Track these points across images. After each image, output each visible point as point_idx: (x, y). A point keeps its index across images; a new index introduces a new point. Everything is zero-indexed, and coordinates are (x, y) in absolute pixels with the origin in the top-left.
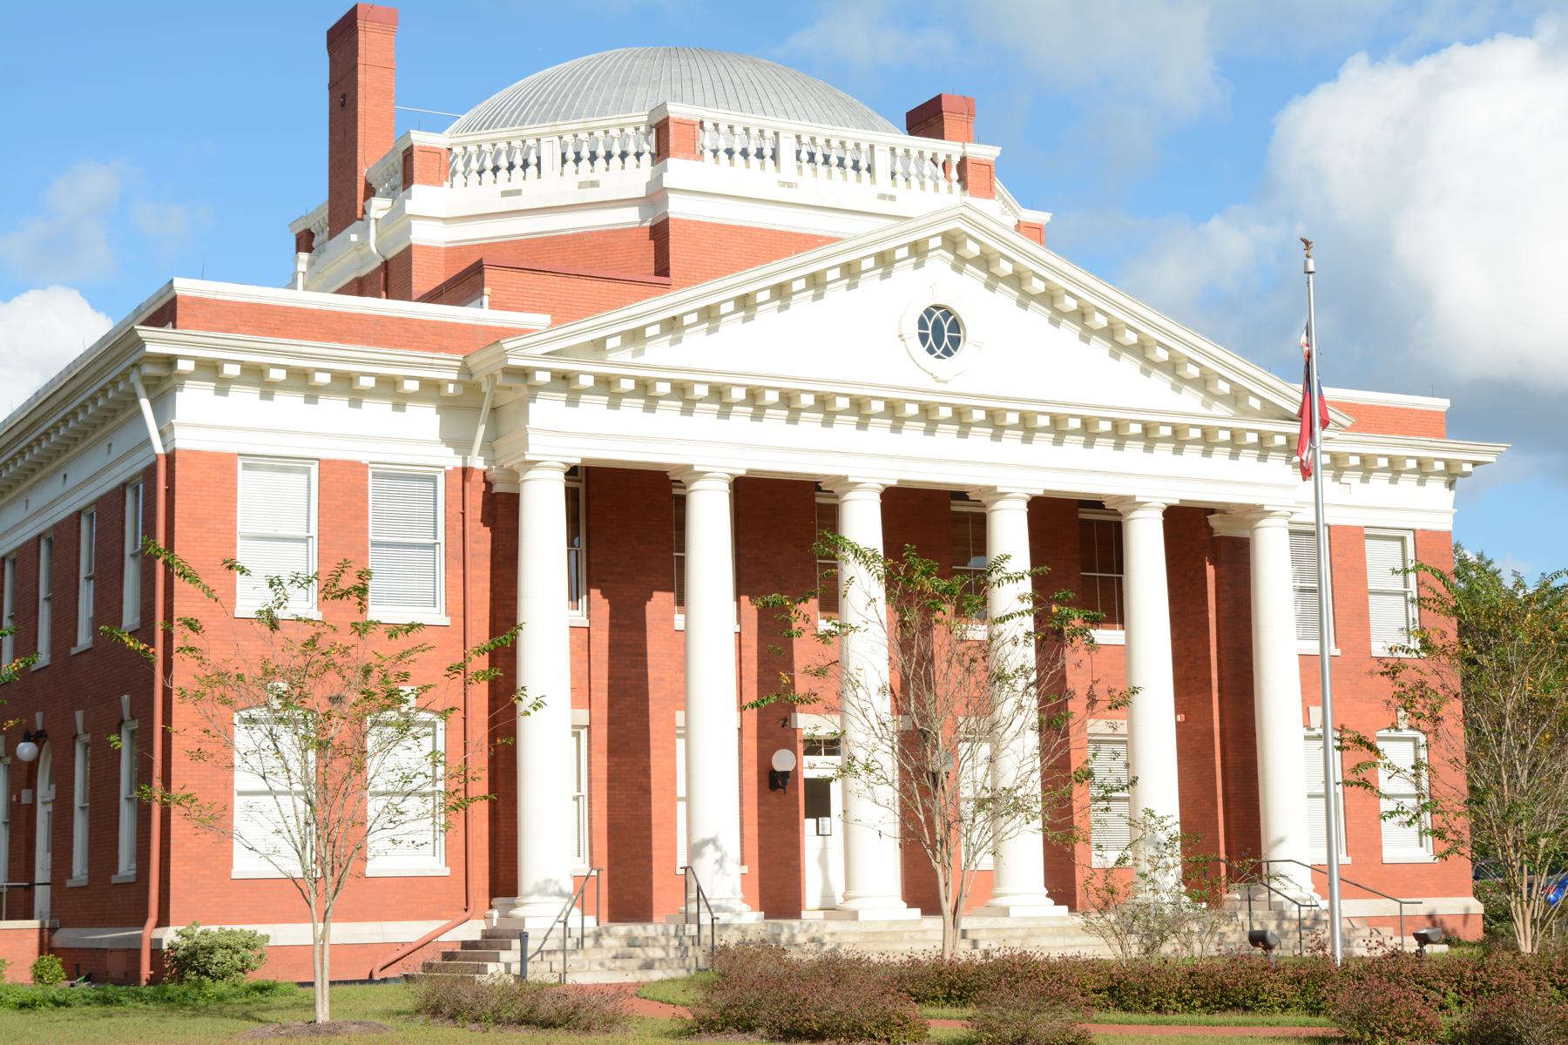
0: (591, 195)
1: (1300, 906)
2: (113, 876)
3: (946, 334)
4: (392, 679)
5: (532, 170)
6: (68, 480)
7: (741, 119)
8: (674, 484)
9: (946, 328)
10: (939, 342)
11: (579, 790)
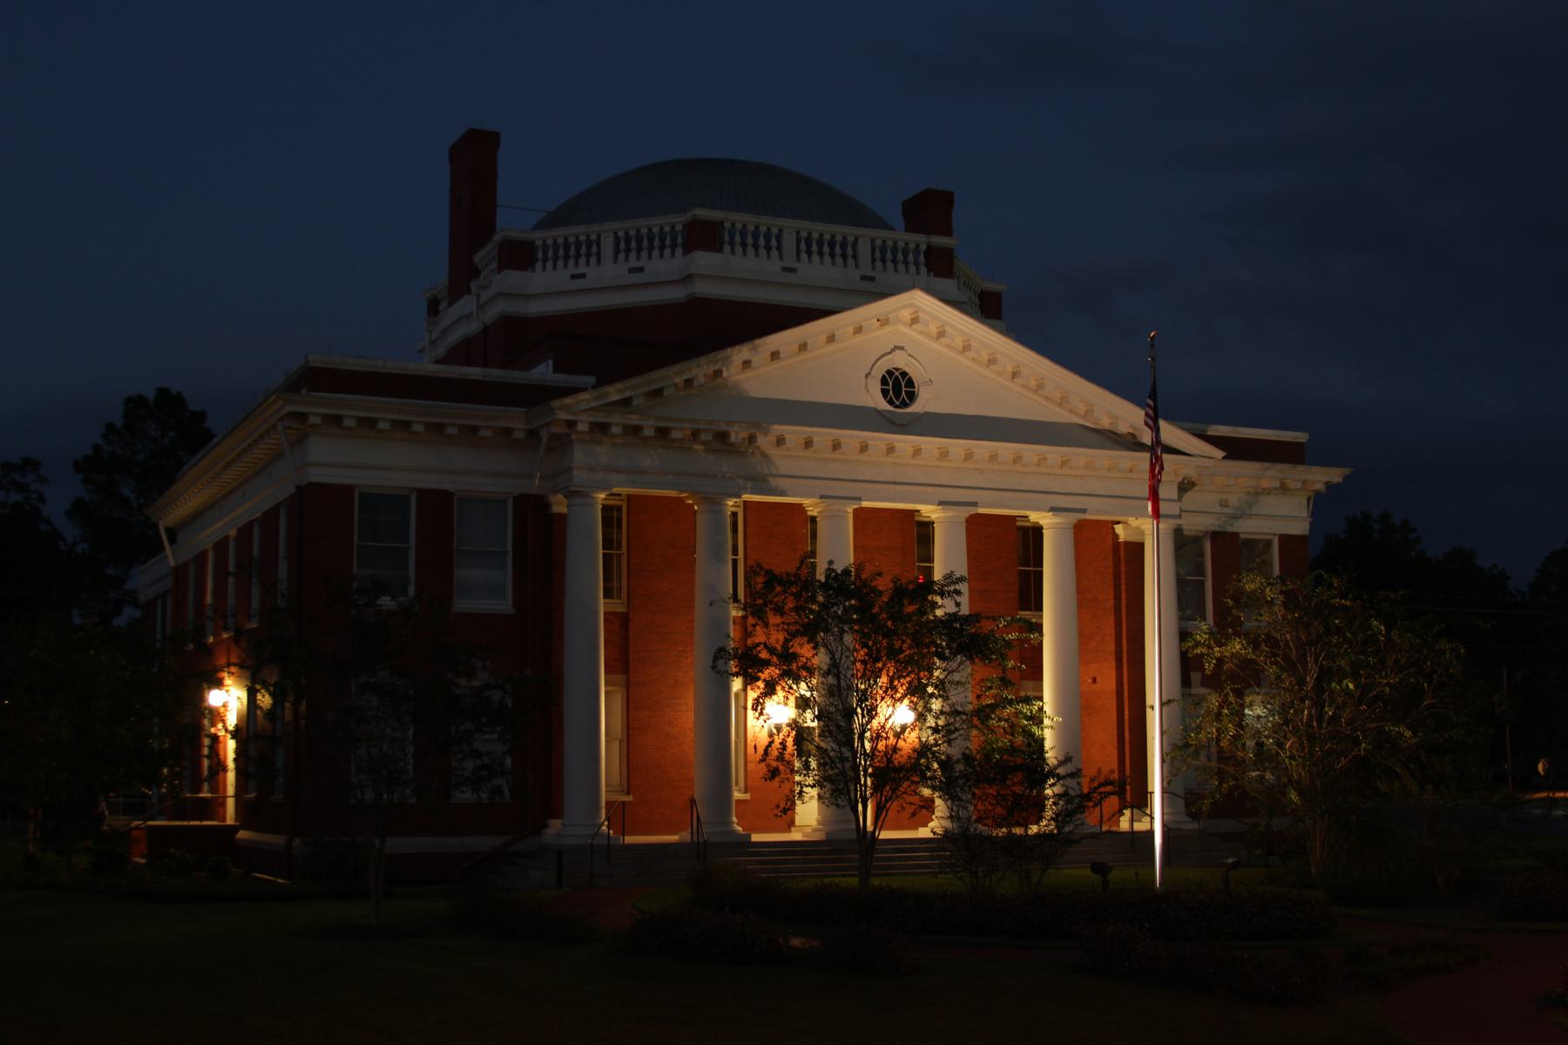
0: (636, 278)
3: (904, 389)
4: (1180, 758)
5: (593, 259)
8: (1018, 519)
9: (903, 385)
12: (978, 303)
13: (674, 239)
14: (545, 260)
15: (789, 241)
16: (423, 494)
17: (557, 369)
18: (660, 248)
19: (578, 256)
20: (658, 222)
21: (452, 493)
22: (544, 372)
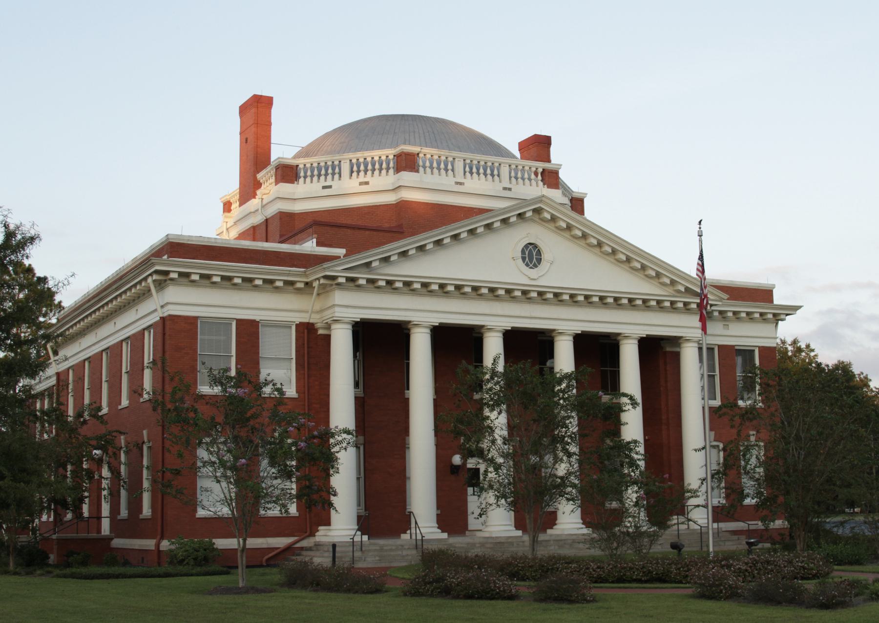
1: (701, 527)
2: (141, 515)
3: (535, 257)
5: (336, 176)
6: (116, 325)
7: (437, 152)
9: (534, 254)
10: (531, 260)
11: (360, 475)
12: (570, 204)
13: (388, 164)
14: (305, 177)
15: (459, 165)
16: (240, 323)
17: (319, 244)
18: (357, 172)
19: (326, 175)
20: (376, 154)
21: (258, 322)
22: (310, 246)
